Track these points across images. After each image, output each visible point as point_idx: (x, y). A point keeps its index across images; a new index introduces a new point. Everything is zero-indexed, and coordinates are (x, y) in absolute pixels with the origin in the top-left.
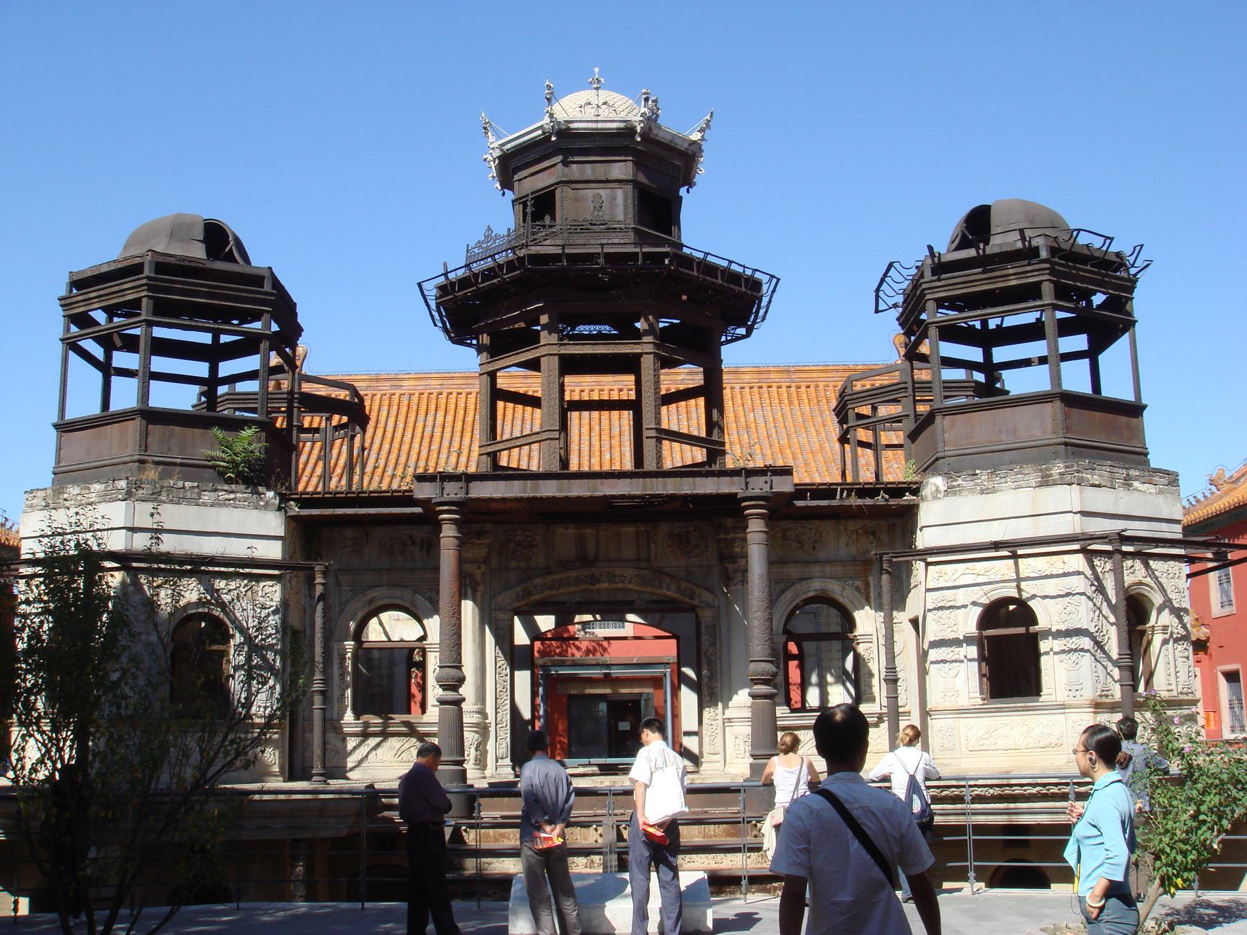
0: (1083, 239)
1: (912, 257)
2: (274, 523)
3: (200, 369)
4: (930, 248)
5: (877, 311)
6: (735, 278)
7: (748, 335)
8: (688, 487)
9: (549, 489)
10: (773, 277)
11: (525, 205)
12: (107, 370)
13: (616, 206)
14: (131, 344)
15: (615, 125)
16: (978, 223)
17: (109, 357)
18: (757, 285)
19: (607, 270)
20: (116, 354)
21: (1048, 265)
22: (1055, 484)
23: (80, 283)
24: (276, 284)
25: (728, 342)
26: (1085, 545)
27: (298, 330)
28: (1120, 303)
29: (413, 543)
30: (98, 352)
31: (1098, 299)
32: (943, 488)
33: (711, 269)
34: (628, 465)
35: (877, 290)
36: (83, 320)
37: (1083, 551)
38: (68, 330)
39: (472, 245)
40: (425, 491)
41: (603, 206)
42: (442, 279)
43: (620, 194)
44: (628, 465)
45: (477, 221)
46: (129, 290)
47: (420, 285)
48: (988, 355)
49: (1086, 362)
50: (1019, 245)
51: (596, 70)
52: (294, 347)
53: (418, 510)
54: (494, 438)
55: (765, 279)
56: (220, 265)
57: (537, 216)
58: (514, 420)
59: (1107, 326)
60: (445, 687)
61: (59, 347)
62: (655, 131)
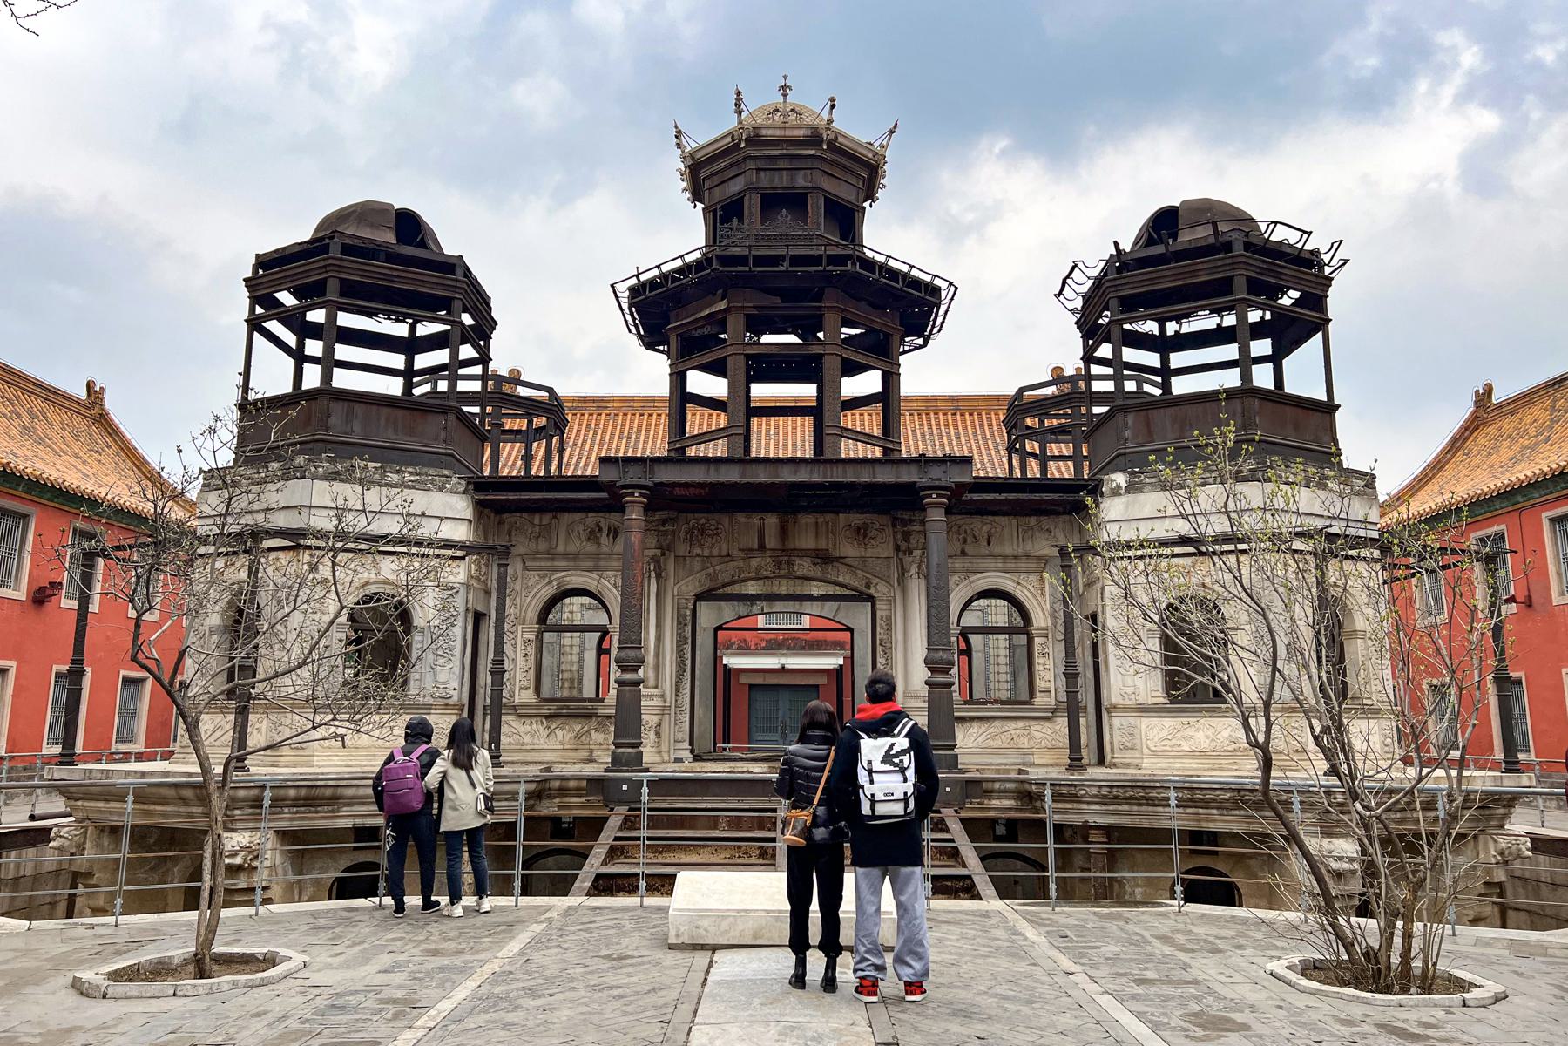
0: (1279, 235)
1: (1096, 258)
2: (461, 506)
3: (397, 361)
4: (1116, 244)
6: (916, 283)
7: (925, 345)
8: (865, 476)
9: (732, 475)
10: (951, 283)
11: (715, 212)
12: (300, 358)
14: (315, 331)
15: (802, 133)
17: (301, 345)
19: (784, 254)
21: (1110, 371)
25: (905, 352)
27: (493, 324)
28: (1315, 300)
30: (290, 339)
32: (1124, 484)
33: (894, 274)
34: (809, 454)
36: (272, 304)
38: (252, 310)
40: (611, 476)
42: (634, 281)
44: (809, 454)
46: (308, 271)
47: (612, 286)
49: (1270, 365)
50: (1212, 240)
52: (487, 338)
53: (604, 495)
54: (683, 432)
55: (943, 285)
56: (408, 250)
57: (726, 219)
58: (699, 420)
59: (1302, 324)
60: (623, 669)
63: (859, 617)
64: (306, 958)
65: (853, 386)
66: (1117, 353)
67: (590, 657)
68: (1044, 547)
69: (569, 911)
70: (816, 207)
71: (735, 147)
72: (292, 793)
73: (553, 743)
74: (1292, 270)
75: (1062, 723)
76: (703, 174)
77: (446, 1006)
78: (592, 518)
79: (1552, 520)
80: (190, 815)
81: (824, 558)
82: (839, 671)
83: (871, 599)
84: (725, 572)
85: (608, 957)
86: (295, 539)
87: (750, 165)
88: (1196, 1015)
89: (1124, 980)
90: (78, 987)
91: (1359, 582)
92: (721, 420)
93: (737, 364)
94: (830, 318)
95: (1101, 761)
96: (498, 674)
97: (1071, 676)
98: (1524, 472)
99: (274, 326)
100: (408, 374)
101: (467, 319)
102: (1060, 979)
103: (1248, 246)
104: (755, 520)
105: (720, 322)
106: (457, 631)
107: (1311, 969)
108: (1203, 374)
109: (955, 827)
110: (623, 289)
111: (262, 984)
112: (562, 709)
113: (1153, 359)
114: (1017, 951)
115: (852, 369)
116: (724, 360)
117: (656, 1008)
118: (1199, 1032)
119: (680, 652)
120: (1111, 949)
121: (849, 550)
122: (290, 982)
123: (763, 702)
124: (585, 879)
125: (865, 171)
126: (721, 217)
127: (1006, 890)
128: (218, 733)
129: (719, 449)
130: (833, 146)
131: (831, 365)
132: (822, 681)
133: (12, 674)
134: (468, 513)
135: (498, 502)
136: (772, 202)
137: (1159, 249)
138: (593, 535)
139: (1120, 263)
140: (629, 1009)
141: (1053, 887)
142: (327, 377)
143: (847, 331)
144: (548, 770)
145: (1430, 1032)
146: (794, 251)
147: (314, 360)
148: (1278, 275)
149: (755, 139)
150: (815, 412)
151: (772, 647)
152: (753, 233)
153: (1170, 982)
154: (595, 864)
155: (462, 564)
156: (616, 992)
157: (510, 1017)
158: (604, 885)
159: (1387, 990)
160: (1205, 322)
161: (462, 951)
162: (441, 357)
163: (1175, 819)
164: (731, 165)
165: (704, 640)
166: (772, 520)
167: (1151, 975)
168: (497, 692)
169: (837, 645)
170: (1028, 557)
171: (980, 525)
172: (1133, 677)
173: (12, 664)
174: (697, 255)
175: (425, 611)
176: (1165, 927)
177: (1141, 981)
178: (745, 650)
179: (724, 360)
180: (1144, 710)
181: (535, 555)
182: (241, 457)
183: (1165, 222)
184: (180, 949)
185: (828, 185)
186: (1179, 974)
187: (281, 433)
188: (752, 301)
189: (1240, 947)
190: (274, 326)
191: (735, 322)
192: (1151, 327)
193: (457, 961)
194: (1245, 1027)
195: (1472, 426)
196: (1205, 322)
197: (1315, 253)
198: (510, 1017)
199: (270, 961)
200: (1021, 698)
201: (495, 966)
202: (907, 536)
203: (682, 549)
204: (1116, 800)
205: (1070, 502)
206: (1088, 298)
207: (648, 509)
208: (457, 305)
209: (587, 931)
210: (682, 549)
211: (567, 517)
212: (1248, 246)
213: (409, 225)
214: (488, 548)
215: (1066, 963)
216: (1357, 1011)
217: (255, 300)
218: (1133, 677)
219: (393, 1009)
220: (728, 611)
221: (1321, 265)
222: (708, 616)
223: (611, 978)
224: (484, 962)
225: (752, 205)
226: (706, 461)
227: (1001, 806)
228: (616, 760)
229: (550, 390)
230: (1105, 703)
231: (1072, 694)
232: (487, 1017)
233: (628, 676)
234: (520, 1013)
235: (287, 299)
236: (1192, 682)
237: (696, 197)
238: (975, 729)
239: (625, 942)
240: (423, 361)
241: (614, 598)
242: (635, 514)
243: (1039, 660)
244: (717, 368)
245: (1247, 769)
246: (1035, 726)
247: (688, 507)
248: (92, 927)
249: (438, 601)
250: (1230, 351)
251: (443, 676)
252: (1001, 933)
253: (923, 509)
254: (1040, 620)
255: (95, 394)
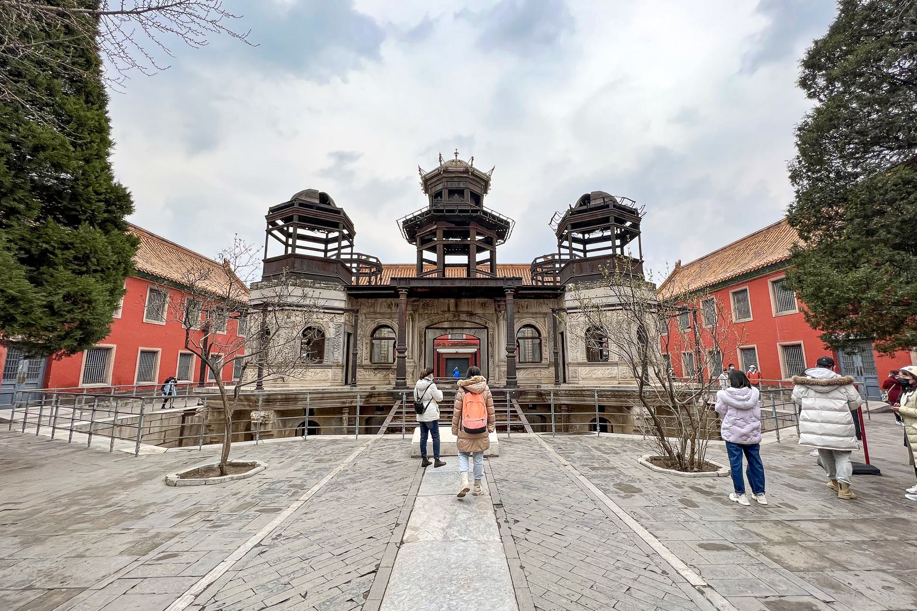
2: (342, 295)
3: (322, 246)
6: (501, 221)
8: (485, 284)
9: (438, 284)
12: (287, 245)
18: (508, 223)
19: (456, 209)
23: (272, 210)
24: (345, 214)
27: (354, 233)
28: (636, 225)
30: (284, 238)
31: (628, 224)
33: (494, 217)
34: (465, 276)
36: (274, 224)
40: (395, 284)
44: (465, 276)
46: (287, 212)
48: (585, 247)
56: (323, 206)
59: (634, 232)
63: (483, 335)
64: (266, 465)
65: (480, 257)
66: (571, 245)
67: (391, 349)
68: (546, 309)
69: (376, 441)
70: (467, 195)
71: (439, 174)
72: (280, 397)
73: (376, 378)
74: (628, 215)
75: (552, 369)
76: (428, 182)
77: (316, 488)
78: (389, 300)
79: (733, 293)
80: (243, 405)
81: (471, 314)
82: (475, 354)
83: (486, 328)
84: (436, 319)
85: (387, 462)
86: (282, 306)
87: (444, 180)
88: (619, 484)
89: (587, 468)
90: (168, 483)
91: (650, 320)
92: (435, 267)
93: (440, 248)
94: (472, 232)
95: (565, 382)
96: (355, 355)
97: (556, 354)
98: (722, 276)
100: (326, 251)
101: (345, 232)
102: (562, 468)
103: (614, 206)
104: (446, 301)
105: (434, 233)
106: (341, 340)
107: (653, 460)
108: (597, 250)
109: (517, 407)
110: (401, 222)
111: (244, 478)
112: (380, 367)
113: (581, 247)
114: (544, 456)
115: (480, 250)
116: (435, 246)
117: (403, 487)
118: (623, 494)
119: (420, 347)
120: (578, 453)
121: (479, 311)
122: (257, 476)
123: (450, 364)
124: (383, 428)
125: (484, 182)
126: (435, 196)
127: (535, 430)
129: (435, 275)
130: (473, 174)
131: (473, 248)
132: (469, 356)
133: (114, 352)
134: (345, 298)
135: (356, 294)
136: (452, 192)
137: (585, 207)
138: (389, 306)
139: (572, 212)
140: (391, 488)
141: (554, 428)
142: (293, 250)
143: (478, 238)
144: (374, 388)
145: (712, 490)
146: (459, 208)
148: (624, 216)
149: (446, 171)
150: (468, 266)
151: (454, 345)
152: (447, 202)
153: (604, 468)
154: (387, 423)
156: (387, 480)
157: (341, 494)
158: (391, 430)
159: (685, 470)
160: (597, 234)
161: (330, 460)
162: (335, 245)
163: (595, 401)
165: (429, 344)
166: (452, 301)
167: (596, 465)
168: (355, 361)
169: (475, 345)
170: (540, 313)
171: (524, 302)
172: (576, 352)
173: (115, 346)
174: (426, 209)
175: (330, 333)
176: (596, 443)
177: (594, 469)
178: (444, 346)
179: (435, 246)
180: (580, 364)
181: (369, 313)
182: (265, 278)
183: (586, 199)
184: (216, 461)
185: (472, 187)
186: (606, 465)
187: (274, 268)
188: (445, 226)
189: (625, 451)
190: (276, 232)
191: (440, 233)
192: (580, 236)
193: (327, 465)
194: (639, 491)
195: (675, 273)
196: (597, 234)
197: (636, 210)
198: (341, 494)
199: (253, 465)
200: (538, 361)
201: (341, 468)
202: (499, 306)
203: (421, 311)
204: (571, 395)
205: (556, 293)
206: (560, 225)
207: (408, 296)
208: (341, 226)
209: (381, 450)
210: (421, 311)
211: (380, 300)
212: (614, 206)
213: (324, 198)
214: (352, 311)
215: (564, 461)
216: (680, 480)
217: (269, 223)
218: (576, 352)
219: (293, 490)
220: (438, 333)
221: (638, 214)
222: (431, 335)
223: (387, 473)
224: (338, 465)
225: (445, 193)
226: (430, 279)
227: (530, 399)
228: (397, 384)
230: (566, 362)
231: (556, 360)
232: (331, 494)
233: (401, 355)
234: (346, 492)
235: (280, 222)
236: (596, 355)
237: (426, 192)
238: (522, 372)
239: (395, 454)
240: (330, 246)
241: (396, 327)
242: (403, 298)
243: (543, 348)
244: (433, 249)
245: (634, 385)
246: (543, 371)
247: (423, 294)
248: (190, 450)
249: (333, 328)
250: (609, 243)
251: (336, 355)
252: (536, 447)
253: (505, 296)
254: (544, 334)
255: (226, 262)
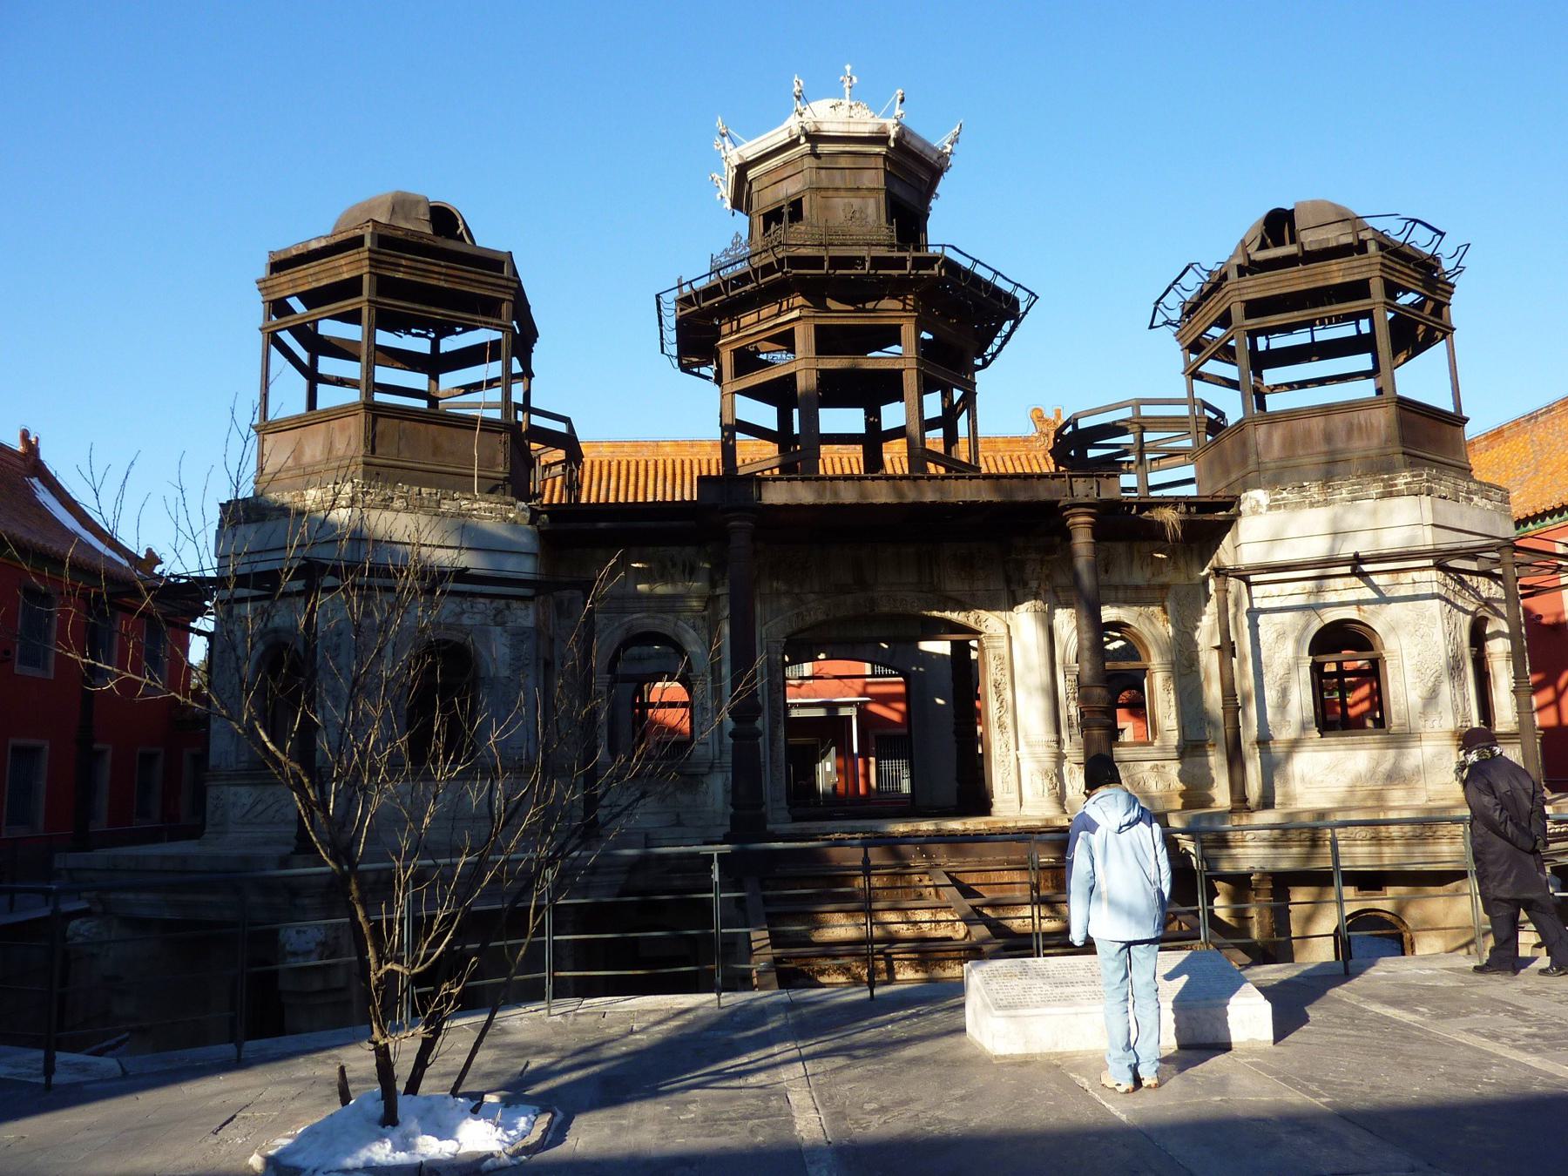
5: (1151, 327)
12: (314, 377)
13: (273, 753)
16: (1278, 224)
17: (314, 362)
20: (321, 359)
22: (1400, 494)
23: (280, 265)
26: (1440, 560)
27: (536, 335)
29: (674, 565)
30: (304, 355)
35: (1158, 302)
37: (1440, 567)
39: (717, 253)
41: (857, 216)
43: (872, 202)
45: (712, 239)
49: (1185, 396)
51: (848, 68)
61: (258, 339)
62: (908, 138)
99: (286, 337)
128: (260, 808)
147: (507, 394)
155: (531, 606)
164: (999, 694)
213: (444, 219)
229: (566, 420)
